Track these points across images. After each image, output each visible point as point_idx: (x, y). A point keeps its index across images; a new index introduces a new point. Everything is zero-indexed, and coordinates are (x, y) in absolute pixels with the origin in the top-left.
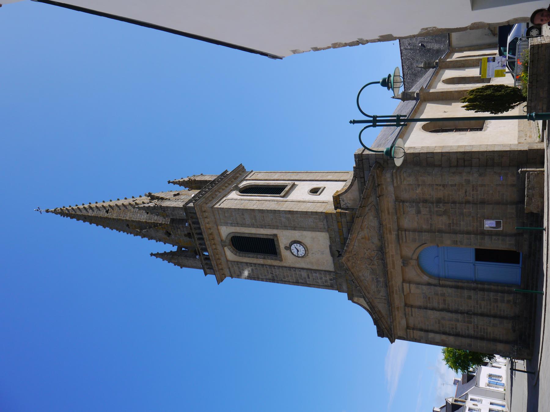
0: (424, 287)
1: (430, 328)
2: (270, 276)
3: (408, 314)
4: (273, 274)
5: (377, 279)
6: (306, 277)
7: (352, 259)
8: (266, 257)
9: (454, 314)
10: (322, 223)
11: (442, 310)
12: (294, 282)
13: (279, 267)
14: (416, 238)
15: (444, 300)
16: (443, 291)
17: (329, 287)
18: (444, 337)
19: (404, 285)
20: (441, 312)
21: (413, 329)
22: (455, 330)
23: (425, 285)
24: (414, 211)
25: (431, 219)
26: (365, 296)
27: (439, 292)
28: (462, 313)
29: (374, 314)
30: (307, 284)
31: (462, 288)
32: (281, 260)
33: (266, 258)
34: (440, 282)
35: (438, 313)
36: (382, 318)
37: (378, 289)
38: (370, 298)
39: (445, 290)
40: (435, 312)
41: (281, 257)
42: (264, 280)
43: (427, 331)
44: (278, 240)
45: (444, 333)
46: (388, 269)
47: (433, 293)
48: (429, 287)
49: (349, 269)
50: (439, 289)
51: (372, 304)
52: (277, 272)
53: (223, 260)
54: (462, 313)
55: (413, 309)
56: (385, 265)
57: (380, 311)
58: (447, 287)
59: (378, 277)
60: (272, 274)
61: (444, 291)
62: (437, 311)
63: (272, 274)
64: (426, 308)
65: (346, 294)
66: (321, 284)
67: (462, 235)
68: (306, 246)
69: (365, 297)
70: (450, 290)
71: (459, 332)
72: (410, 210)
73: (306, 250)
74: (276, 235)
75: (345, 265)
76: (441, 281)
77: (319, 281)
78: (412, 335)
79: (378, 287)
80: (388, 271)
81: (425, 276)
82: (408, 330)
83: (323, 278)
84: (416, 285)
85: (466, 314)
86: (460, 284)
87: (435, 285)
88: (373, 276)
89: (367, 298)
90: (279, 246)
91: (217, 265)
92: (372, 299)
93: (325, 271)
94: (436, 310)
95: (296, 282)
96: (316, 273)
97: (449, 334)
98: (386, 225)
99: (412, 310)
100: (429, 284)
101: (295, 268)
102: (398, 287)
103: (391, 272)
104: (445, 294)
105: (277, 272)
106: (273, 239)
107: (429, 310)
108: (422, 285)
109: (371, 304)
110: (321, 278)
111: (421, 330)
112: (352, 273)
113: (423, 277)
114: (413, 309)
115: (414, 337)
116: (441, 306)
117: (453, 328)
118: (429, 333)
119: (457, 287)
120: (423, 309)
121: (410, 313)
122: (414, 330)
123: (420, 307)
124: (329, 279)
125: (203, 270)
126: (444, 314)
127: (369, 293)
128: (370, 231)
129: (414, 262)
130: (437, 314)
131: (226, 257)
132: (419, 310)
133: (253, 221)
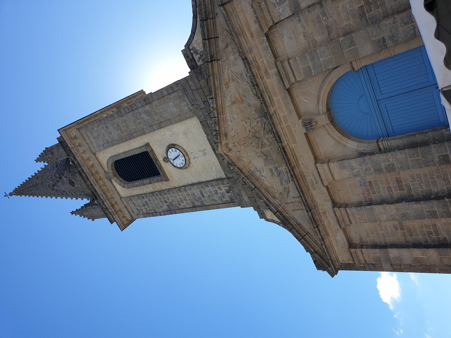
0: (354, 163)
1: (389, 240)
2: (165, 207)
3: (343, 220)
4: (167, 203)
5: (276, 169)
6: (200, 195)
7: (234, 145)
8: (152, 181)
9: (422, 202)
10: (185, 103)
11: (399, 200)
12: (191, 207)
13: (169, 190)
14: (309, 67)
15: (398, 181)
16: (389, 161)
17: (229, 203)
18: (417, 253)
19: (318, 168)
20: (397, 205)
21: (362, 247)
22: (435, 237)
23: (355, 158)
24: (288, 9)
25: (324, 14)
26: (268, 202)
27: (383, 165)
28: (438, 197)
29: (291, 229)
30: (205, 206)
31: (424, 144)
32: (167, 180)
33: (152, 182)
34: (378, 145)
35: (393, 206)
36: (306, 235)
37: (284, 187)
38: (277, 205)
39: (391, 158)
40: (387, 207)
41: (165, 175)
42: (162, 213)
43: (384, 246)
44: (152, 150)
45: (417, 245)
46: (284, 145)
47: (372, 169)
48: (361, 159)
49: (232, 162)
50: (380, 158)
51: (284, 214)
52: (170, 197)
53: (117, 199)
54: (438, 197)
55: (348, 209)
56: (278, 138)
57: (299, 225)
58: (394, 150)
59: (276, 165)
60: (166, 202)
61: (391, 160)
62: (390, 204)
63: (166, 202)
64: (370, 203)
65: (252, 207)
66: (220, 202)
67: (391, 20)
68: (183, 148)
69: (269, 204)
70: (400, 155)
71: (445, 238)
72: (281, 10)
73: (185, 154)
74: (148, 145)
75: (226, 157)
76: (380, 143)
77: (216, 197)
78: (361, 258)
79: (284, 183)
80: (286, 149)
81: (350, 141)
82: (353, 250)
83: (219, 191)
84: (339, 163)
85: (448, 198)
86: (419, 138)
87: (372, 154)
88: (271, 167)
89: (273, 206)
90: (157, 160)
91: (112, 206)
92: (282, 206)
93: (217, 180)
94: (388, 203)
95: (193, 207)
96: (208, 187)
97: (427, 246)
98: (255, 61)
99: (346, 210)
100: (362, 154)
101: (184, 186)
102: (313, 175)
103: (292, 150)
104: (393, 165)
105: (170, 197)
106: (147, 151)
107: (375, 205)
108: (348, 159)
109: (281, 213)
110: (216, 193)
111: (375, 246)
112: (238, 168)
113: (348, 145)
114: (348, 209)
115: (365, 260)
116: (396, 193)
117: (430, 233)
118: (388, 249)
119: (413, 146)
120: (364, 206)
121: (346, 219)
122: (363, 248)
123: (360, 205)
124: (225, 191)
125: (107, 218)
126: (403, 206)
127: (274, 197)
128: (237, 83)
129: (323, 120)
130: (392, 209)
131: (118, 193)
132: (359, 208)
133: (119, 132)
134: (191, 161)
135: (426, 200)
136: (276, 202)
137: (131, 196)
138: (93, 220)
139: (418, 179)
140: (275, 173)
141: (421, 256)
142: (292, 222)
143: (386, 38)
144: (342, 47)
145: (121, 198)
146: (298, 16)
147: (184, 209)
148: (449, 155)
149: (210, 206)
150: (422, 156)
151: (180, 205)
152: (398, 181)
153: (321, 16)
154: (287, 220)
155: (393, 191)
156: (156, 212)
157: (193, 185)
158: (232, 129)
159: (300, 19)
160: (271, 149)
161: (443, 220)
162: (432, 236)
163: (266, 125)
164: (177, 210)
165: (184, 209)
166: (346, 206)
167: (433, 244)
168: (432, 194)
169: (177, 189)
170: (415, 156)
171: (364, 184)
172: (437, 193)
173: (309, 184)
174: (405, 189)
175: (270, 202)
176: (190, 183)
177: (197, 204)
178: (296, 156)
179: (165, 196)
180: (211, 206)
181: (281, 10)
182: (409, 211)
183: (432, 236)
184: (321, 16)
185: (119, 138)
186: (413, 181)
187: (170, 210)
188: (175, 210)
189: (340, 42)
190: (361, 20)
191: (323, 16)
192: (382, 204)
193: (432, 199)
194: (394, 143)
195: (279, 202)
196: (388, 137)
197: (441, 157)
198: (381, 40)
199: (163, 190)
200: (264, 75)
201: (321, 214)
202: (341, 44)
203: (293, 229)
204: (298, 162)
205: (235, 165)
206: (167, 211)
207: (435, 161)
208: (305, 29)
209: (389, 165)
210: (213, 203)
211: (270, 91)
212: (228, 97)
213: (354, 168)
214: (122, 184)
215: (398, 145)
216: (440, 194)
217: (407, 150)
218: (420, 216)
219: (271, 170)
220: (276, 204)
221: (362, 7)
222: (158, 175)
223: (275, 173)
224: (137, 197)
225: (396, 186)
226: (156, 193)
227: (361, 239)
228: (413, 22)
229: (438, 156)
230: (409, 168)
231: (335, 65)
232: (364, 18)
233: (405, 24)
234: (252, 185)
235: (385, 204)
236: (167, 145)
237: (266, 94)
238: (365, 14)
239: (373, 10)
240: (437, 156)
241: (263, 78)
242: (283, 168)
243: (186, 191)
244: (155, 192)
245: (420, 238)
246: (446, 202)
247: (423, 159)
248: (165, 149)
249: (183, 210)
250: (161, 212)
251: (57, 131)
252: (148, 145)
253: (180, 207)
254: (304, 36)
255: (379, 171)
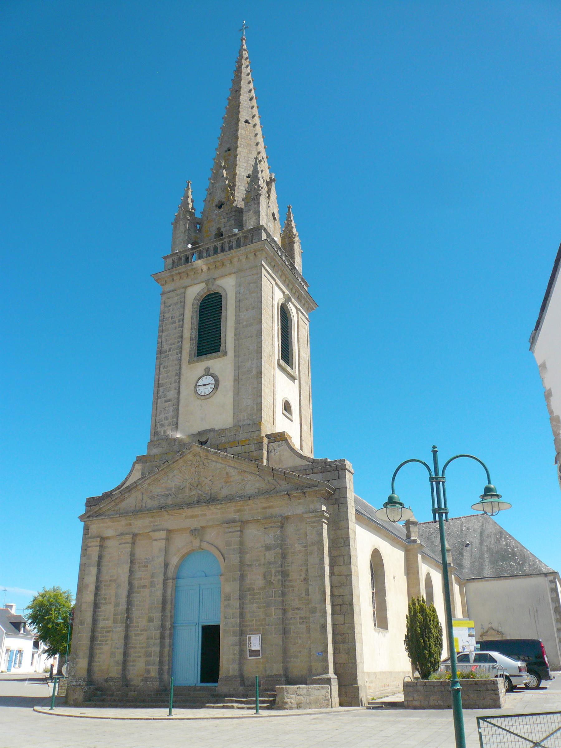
1: (104, 569)
4: (169, 352)
5: (171, 495)
11: (130, 584)
12: (159, 381)
15: (144, 587)
18: (92, 588)
21: (101, 546)
25: (259, 565)
26: (145, 479)
27: (155, 580)
30: (157, 399)
31: (163, 609)
32: (190, 362)
35: (127, 579)
38: (142, 486)
41: (194, 362)
43: (99, 565)
45: (97, 589)
48: (163, 565)
49: (183, 456)
53: (186, 281)
56: (190, 505)
58: (163, 589)
60: (170, 350)
61: (158, 586)
62: (129, 578)
63: (170, 350)
72: (271, 536)
74: (225, 354)
81: (177, 560)
85: (126, 616)
86: (169, 606)
87: (165, 573)
91: (179, 273)
94: (129, 576)
96: (173, 411)
97: (96, 595)
100: (166, 565)
101: (179, 382)
108: (165, 556)
110: (166, 418)
112: (177, 460)
116: (136, 583)
117: (105, 599)
119: (164, 602)
120: (131, 558)
123: (132, 554)
126: (126, 586)
127: (149, 484)
132: (129, 554)
133: (245, 323)
134: (200, 401)
135: (127, 602)
136: (145, 485)
137: (184, 303)
138: (172, 224)
140: (168, 492)
141: (89, 589)
142: (127, 495)
145: (186, 288)
147: (159, 370)
149: (156, 405)
151: (164, 367)
152: (144, 587)
153: (259, 562)
154: (129, 491)
156: (162, 331)
157: (179, 393)
160: (186, 496)
161: (112, 610)
162: (103, 600)
163: (204, 498)
164: (160, 362)
165: (159, 370)
166: (133, 543)
167: (97, 599)
168: (131, 606)
169: (178, 372)
171: (147, 561)
172: (132, 609)
175: (145, 481)
176: (181, 390)
177: (161, 389)
179: (175, 352)
180: (155, 408)
181: (271, 536)
183: (103, 600)
184: (259, 562)
185: (240, 320)
187: (162, 353)
188: (160, 359)
192: (130, 571)
193: (128, 606)
194: (169, 590)
195: (144, 487)
199: (181, 351)
203: (120, 494)
205: (180, 458)
206: (161, 347)
210: (159, 410)
214: (198, 297)
216: (130, 612)
217: (161, 598)
218: (117, 596)
219: (171, 489)
220: (144, 484)
222: (198, 353)
223: (168, 492)
224: (182, 312)
226: (181, 342)
227: (107, 547)
230: (150, 596)
234: (161, 469)
235: (129, 574)
236: (220, 379)
242: (169, 501)
243: (175, 382)
244: (182, 341)
245: (103, 592)
246: (124, 615)
248: (217, 373)
249: (158, 370)
250: (162, 338)
253: (162, 366)
255: (153, 576)
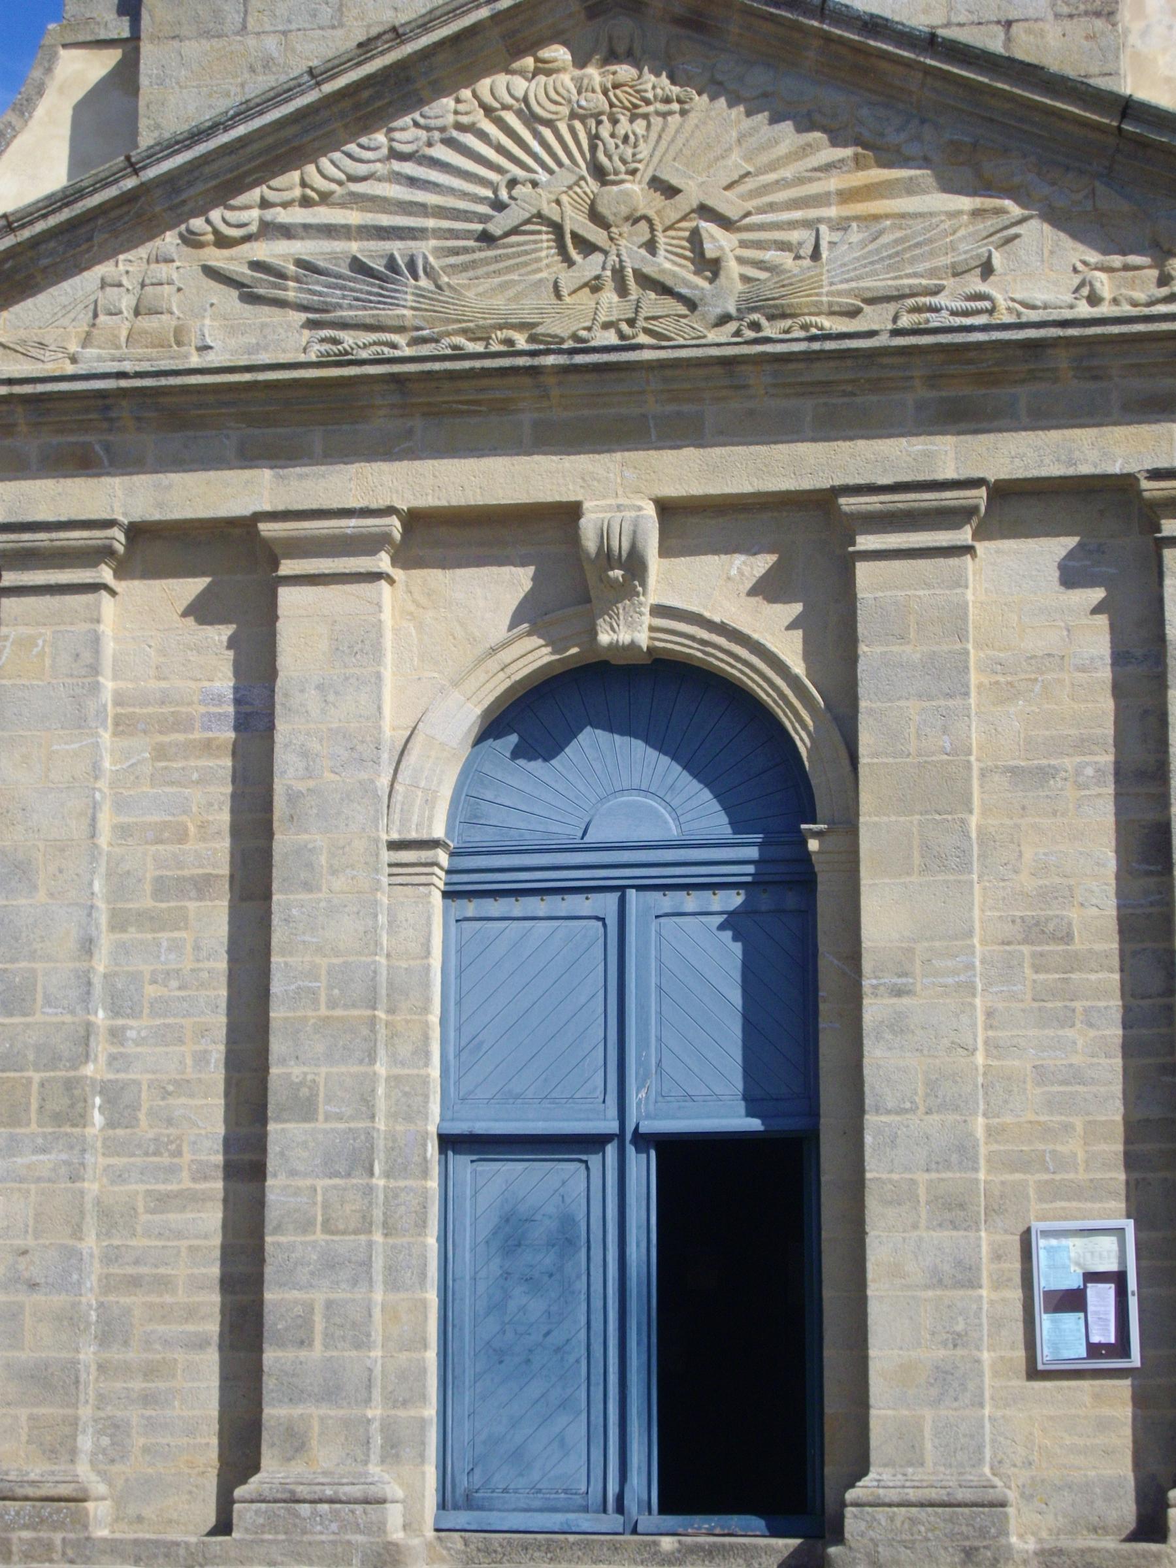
16: (334, 872)
61: (338, 883)
139: (205, 975)
143: (905, 1000)
144: (937, 817)
146: (1146, 657)
148: (312, 1125)
150: (328, 1017)
155: (160, 847)
158: (719, 77)
159: (1131, 663)
170: (336, 991)
173: (280, 430)
174: (164, 905)
178: (462, 412)
182: (41, 896)
186: (197, 948)
189: (960, 816)
190: (1019, 920)
191: (1099, 770)
196: (442, 887)
197: (304, 1092)
198: (904, 980)
200: (944, 394)
201: (82, 439)
202: (949, 817)
204: (424, 414)
207: (292, 1063)
208: (1082, 669)
209: (310, 866)
211: (855, 395)
212: (903, 136)
213: (331, 698)
215: (399, 927)
221: (1068, 938)
225: (180, 865)
228: (325, 456)
229: (314, 1081)
231: (869, 760)
232: (1020, 937)
233: (932, 1086)
237: (849, 375)
238: (1032, 943)
239: (1035, 977)
240: (317, 1078)
241: (932, 387)
247: (312, 1021)
251: (1038, 1385)
252: (1046, 1293)
254: (1049, 655)
